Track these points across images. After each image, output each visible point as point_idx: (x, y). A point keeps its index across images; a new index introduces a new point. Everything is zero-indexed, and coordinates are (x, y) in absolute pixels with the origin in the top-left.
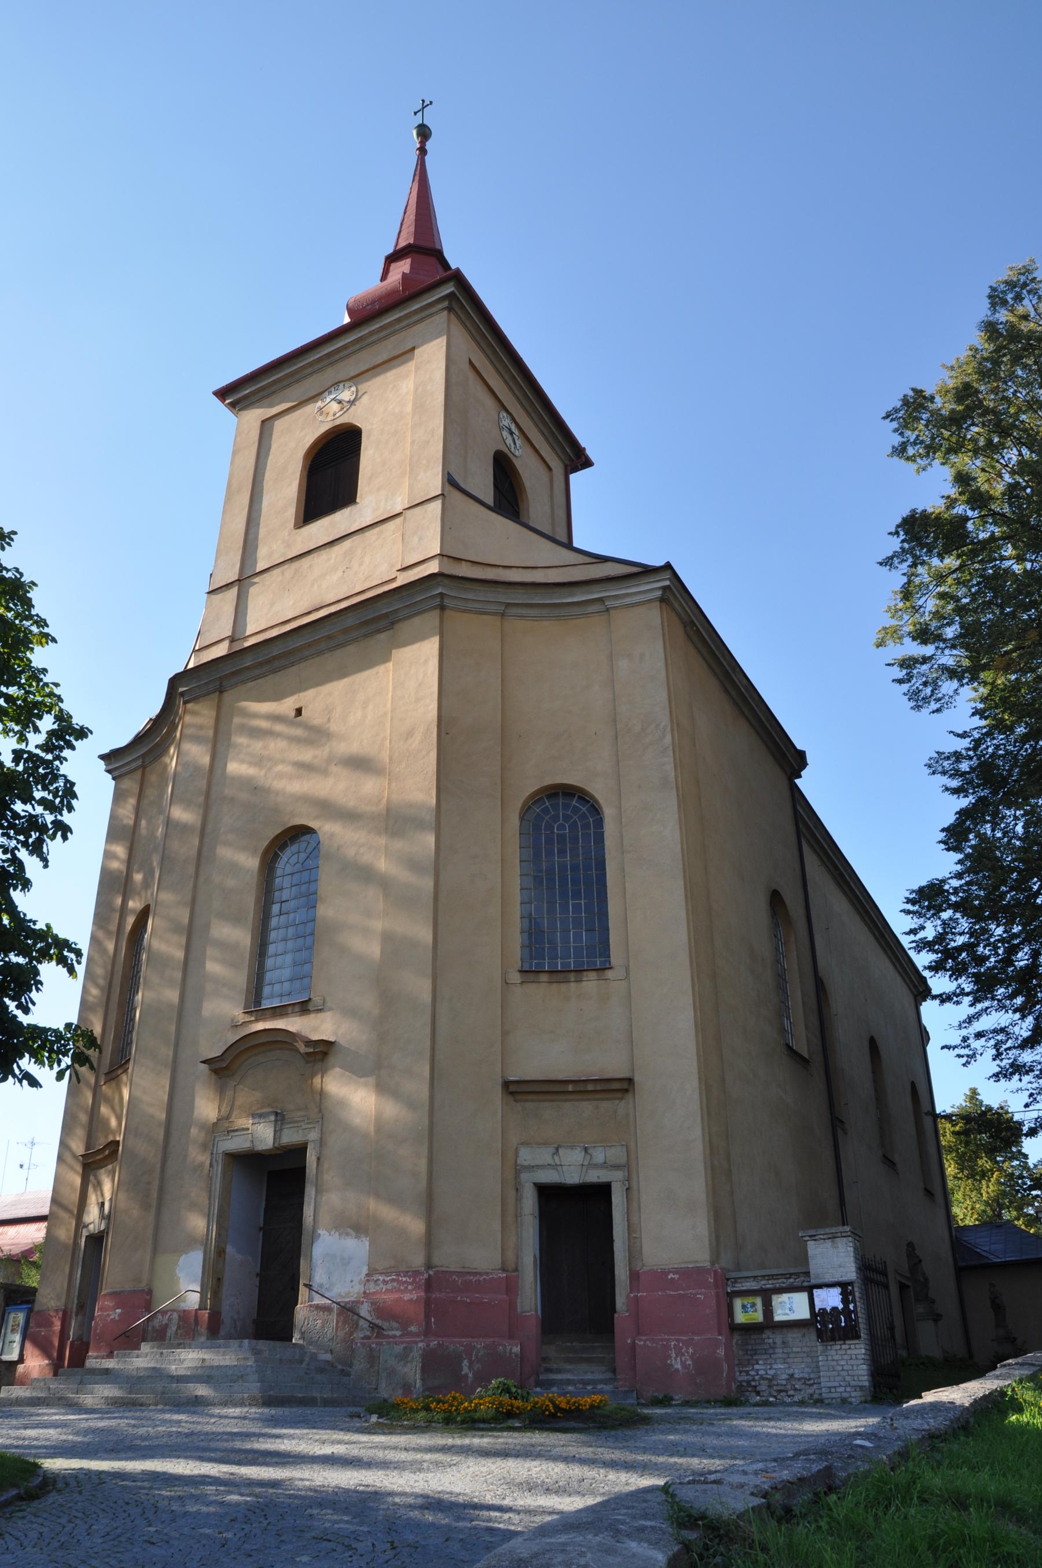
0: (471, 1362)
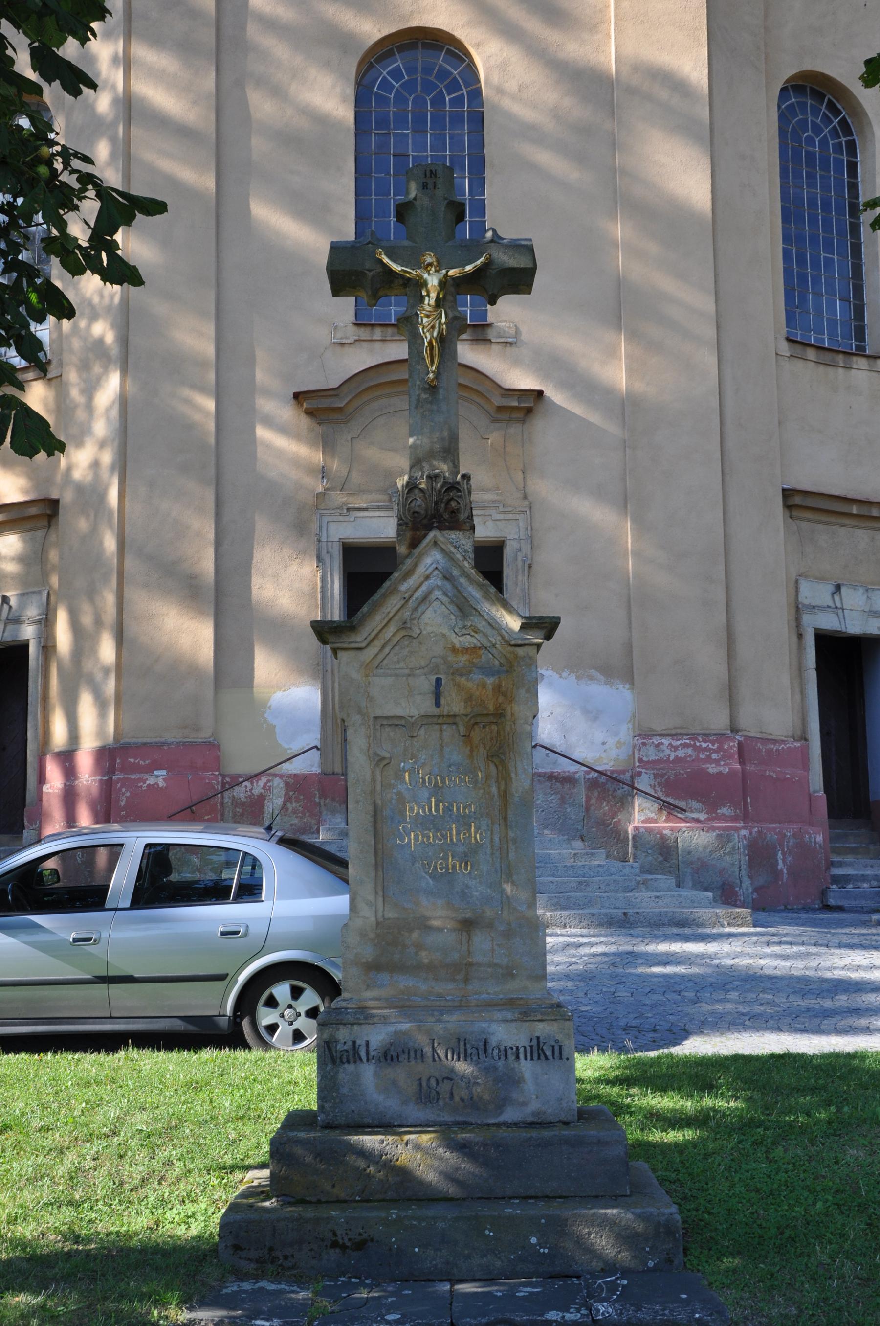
0: (784, 854)
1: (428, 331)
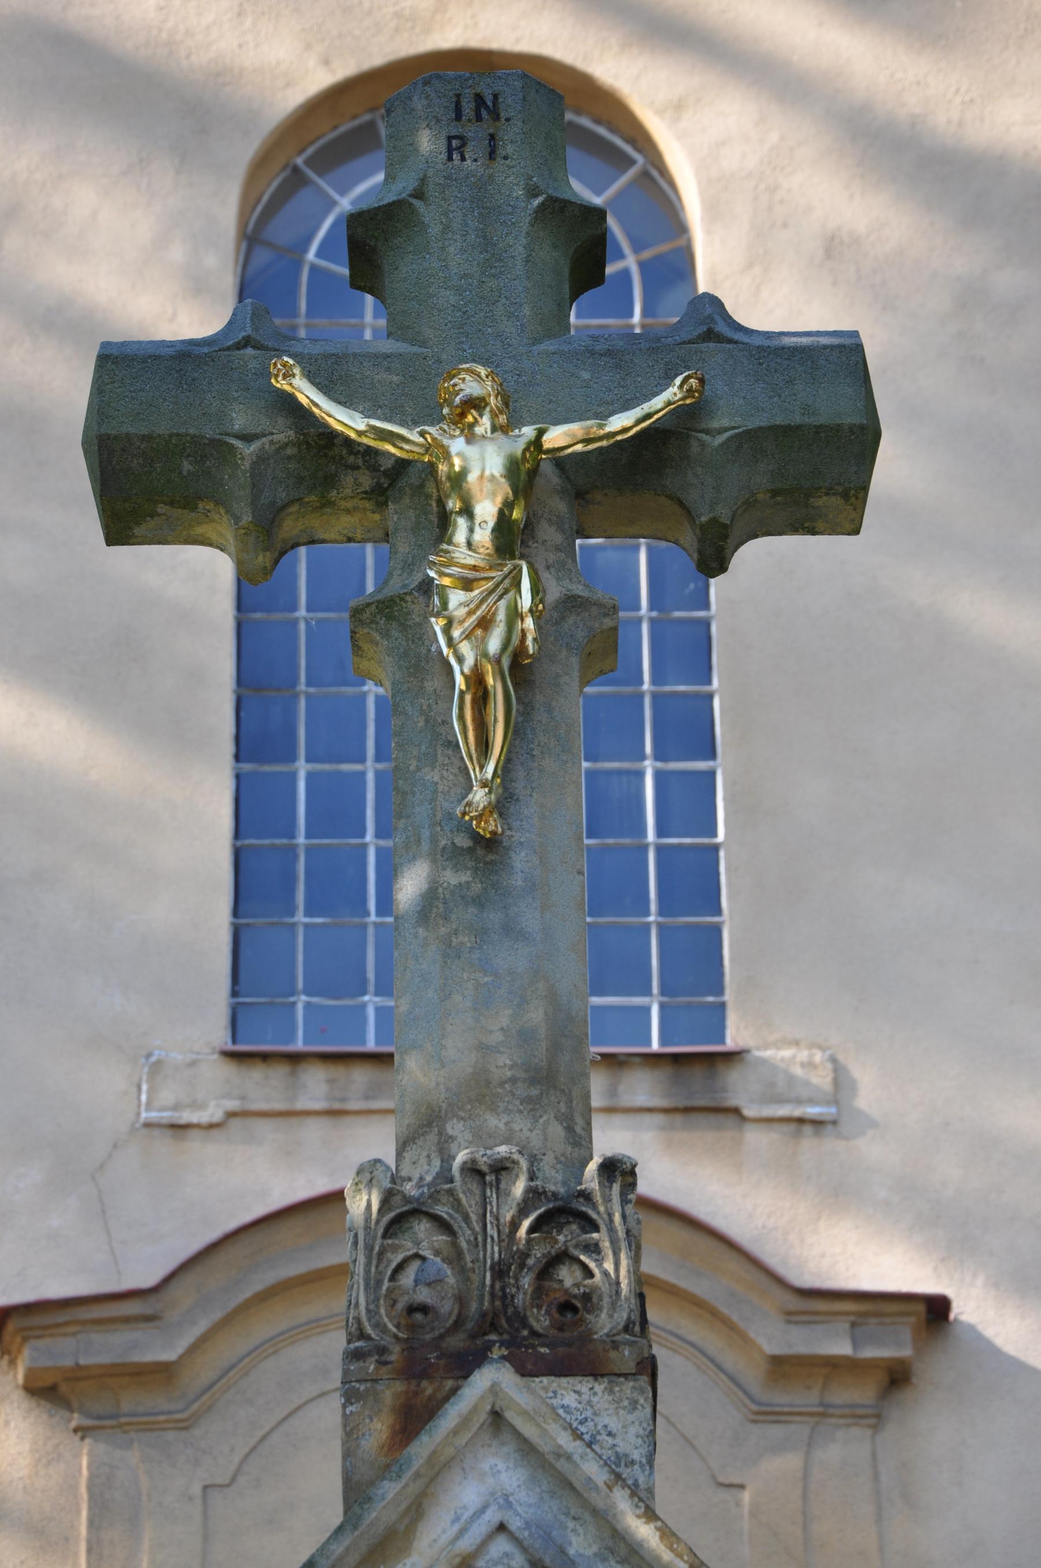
1: (468, 636)
